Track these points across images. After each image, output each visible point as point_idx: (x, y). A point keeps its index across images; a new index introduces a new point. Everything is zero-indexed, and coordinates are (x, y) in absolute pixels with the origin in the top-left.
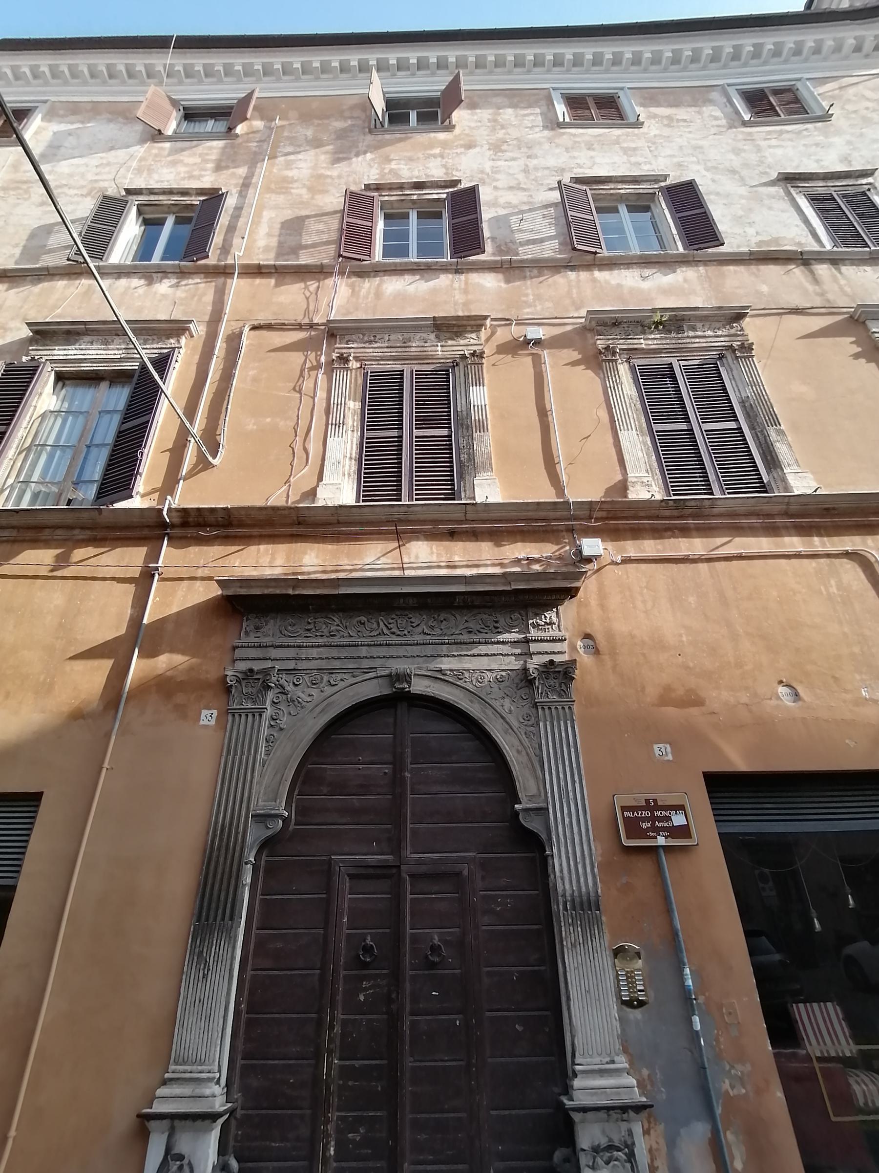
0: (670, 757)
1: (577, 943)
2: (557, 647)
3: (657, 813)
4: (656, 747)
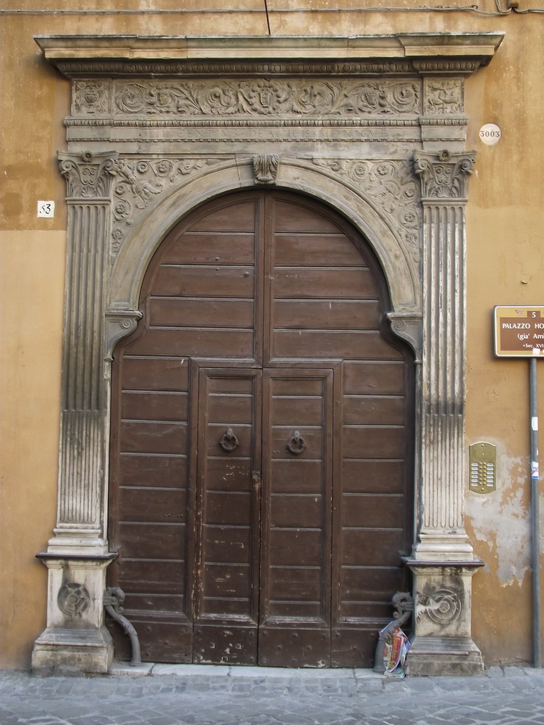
2: (456, 132)
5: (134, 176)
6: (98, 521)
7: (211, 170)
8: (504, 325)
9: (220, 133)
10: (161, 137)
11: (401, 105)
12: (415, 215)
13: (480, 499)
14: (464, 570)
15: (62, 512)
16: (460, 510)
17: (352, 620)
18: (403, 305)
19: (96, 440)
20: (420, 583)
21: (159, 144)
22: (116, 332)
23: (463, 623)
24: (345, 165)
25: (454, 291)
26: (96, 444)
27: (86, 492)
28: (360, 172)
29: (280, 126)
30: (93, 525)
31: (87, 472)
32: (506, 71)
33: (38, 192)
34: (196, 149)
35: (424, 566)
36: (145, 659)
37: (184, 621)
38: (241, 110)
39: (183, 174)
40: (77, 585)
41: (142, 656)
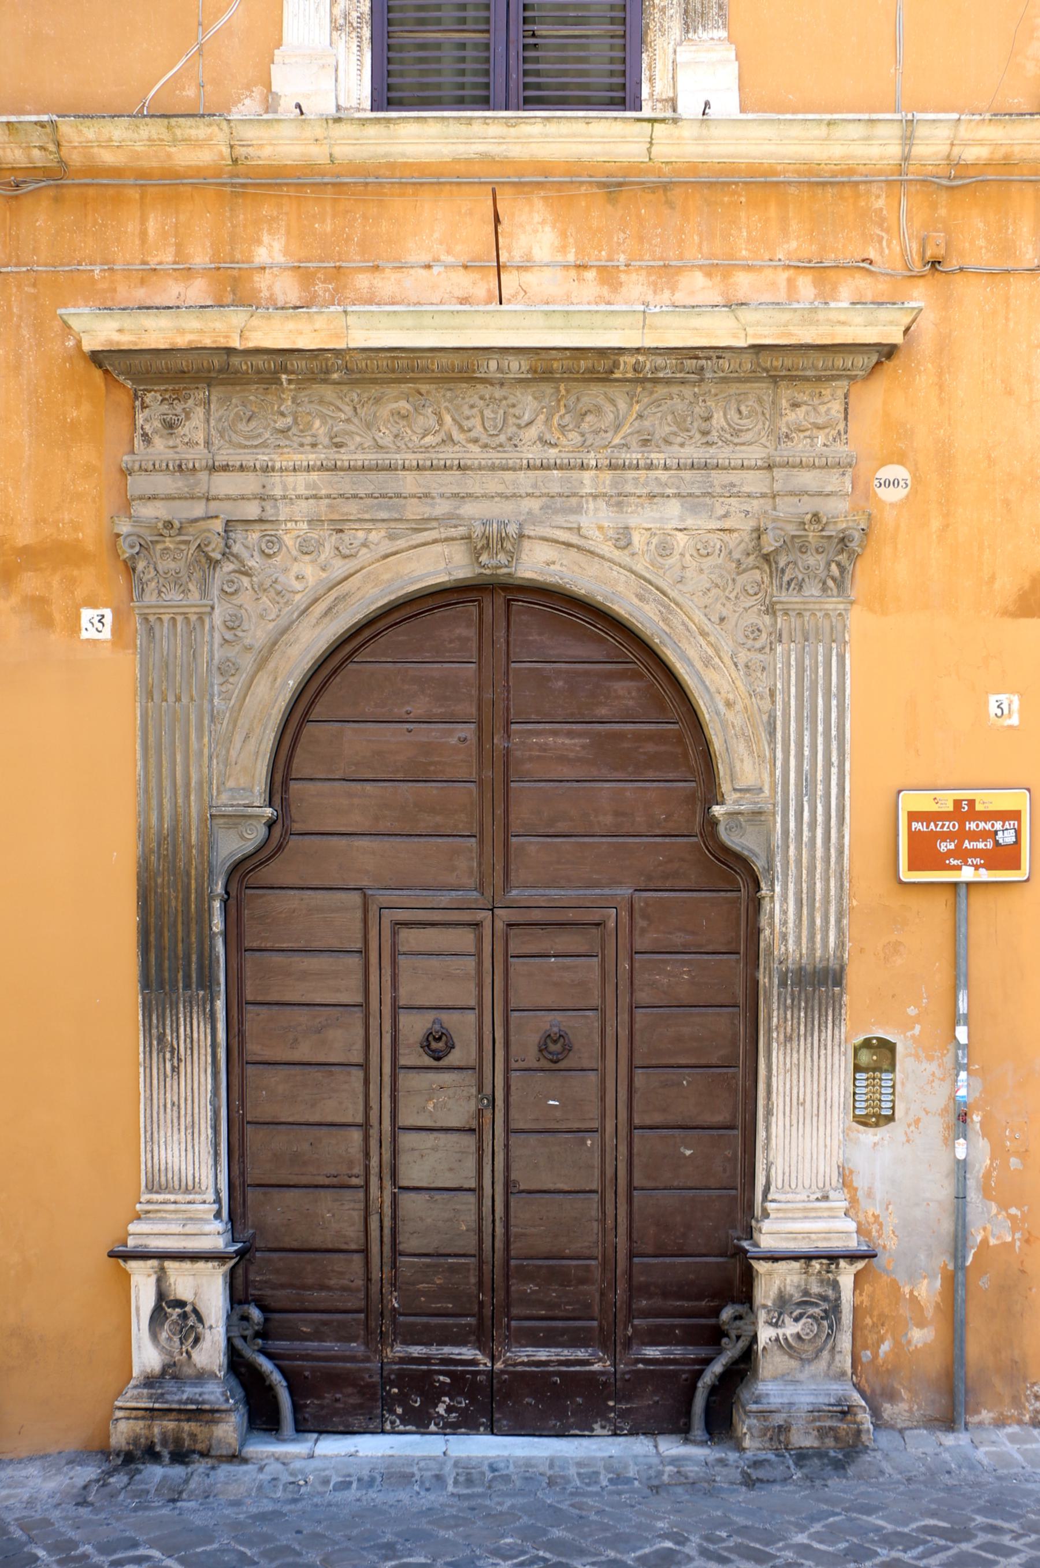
0: (1015, 721)
1: (795, 1035)
2: (833, 481)
3: (972, 826)
4: (993, 699)
5: (254, 562)
6: (211, 1190)
7: (394, 549)
8: (917, 826)
9: (409, 483)
10: (301, 491)
11: (737, 433)
12: (762, 627)
13: (868, 1136)
14: (842, 1263)
15: (150, 1175)
16: (834, 1159)
17: (652, 1352)
18: (740, 790)
19: (202, 1044)
20: (765, 1292)
21: (299, 502)
22: (233, 845)
23: (838, 1357)
24: (638, 539)
25: (828, 764)
26: (202, 1051)
27: (189, 1137)
28: (665, 549)
29: (521, 469)
30: (204, 1197)
31: (189, 1102)
32: (920, 372)
33: (80, 593)
34: (367, 512)
35: (774, 1258)
36: (301, 1428)
37: (367, 1359)
38: (449, 439)
39: (345, 557)
40: (181, 1304)
41: (296, 1421)
